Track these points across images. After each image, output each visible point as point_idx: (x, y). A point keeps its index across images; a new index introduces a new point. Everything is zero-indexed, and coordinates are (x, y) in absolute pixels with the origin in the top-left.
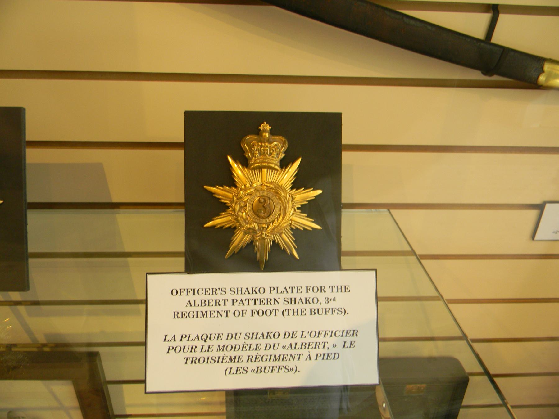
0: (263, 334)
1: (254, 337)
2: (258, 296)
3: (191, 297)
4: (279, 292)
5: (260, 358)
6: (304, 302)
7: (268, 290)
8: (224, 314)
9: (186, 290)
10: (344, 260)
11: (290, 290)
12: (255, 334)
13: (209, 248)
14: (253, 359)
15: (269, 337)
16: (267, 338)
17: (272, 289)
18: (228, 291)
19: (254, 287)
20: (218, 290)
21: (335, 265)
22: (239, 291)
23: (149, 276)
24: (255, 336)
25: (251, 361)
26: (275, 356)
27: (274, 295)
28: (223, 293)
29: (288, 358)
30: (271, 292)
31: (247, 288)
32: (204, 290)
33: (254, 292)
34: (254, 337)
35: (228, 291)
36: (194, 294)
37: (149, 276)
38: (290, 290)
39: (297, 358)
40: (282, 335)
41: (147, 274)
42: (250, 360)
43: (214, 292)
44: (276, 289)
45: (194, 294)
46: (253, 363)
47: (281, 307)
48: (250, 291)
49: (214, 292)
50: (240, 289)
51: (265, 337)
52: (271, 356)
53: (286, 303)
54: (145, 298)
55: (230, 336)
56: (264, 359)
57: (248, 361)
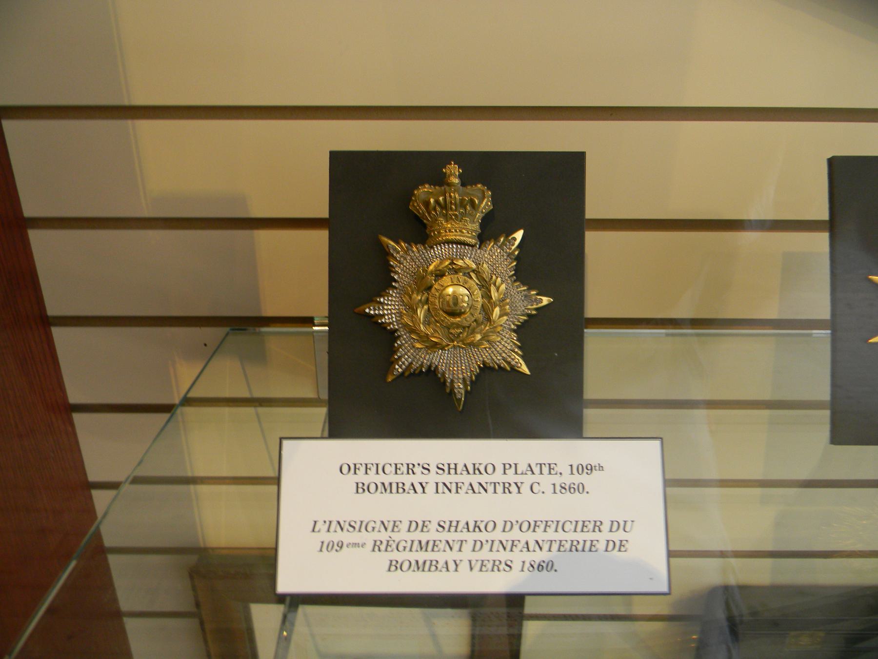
0: (467, 524)
1: (453, 529)
2: (484, 478)
3: (361, 477)
4: (519, 472)
5: (394, 546)
6: (471, 471)
7: (500, 469)
8: (490, 489)
9: (364, 466)
10: (590, 414)
11: (536, 470)
12: (454, 524)
13: (380, 391)
14: (383, 547)
15: (477, 529)
16: (474, 531)
17: (507, 466)
18: (433, 469)
19: (477, 462)
20: (416, 465)
21: (569, 425)
22: (452, 468)
23: (285, 443)
24: (453, 526)
25: (379, 550)
26: (420, 542)
27: (511, 477)
28: (426, 472)
29: (442, 546)
30: (505, 473)
31: (465, 466)
32: (394, 466)
33: (477, 472)
34: (453, 529)
35: (433, 469)
36: (377, 473)
37: (285, 443)
38: (536, 470)
39: (456, 547)
40: (500, 526)
41: (281, 439)
42: (377, 548)
43: (410, 469)
44: (513, 466)
45: (377, 473)
46: (383, 553)
47: (432, 478)
48: (471, 470)
49: (410, 469)
50: (452, 466)
51: (471, 529)
52: (413, 541)
53: (440, 472)
54: (277, 475)
55: (414, 525)
56: (401, 548)
57: (373, 550)
